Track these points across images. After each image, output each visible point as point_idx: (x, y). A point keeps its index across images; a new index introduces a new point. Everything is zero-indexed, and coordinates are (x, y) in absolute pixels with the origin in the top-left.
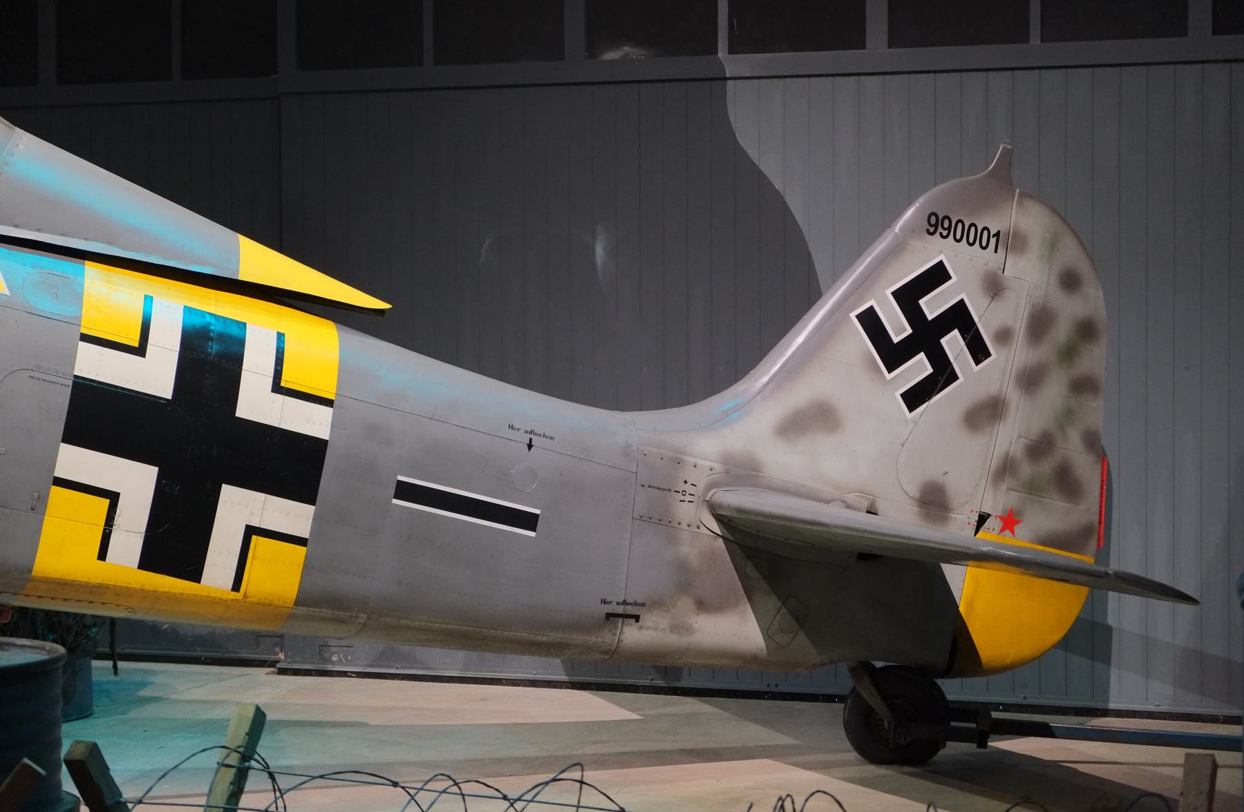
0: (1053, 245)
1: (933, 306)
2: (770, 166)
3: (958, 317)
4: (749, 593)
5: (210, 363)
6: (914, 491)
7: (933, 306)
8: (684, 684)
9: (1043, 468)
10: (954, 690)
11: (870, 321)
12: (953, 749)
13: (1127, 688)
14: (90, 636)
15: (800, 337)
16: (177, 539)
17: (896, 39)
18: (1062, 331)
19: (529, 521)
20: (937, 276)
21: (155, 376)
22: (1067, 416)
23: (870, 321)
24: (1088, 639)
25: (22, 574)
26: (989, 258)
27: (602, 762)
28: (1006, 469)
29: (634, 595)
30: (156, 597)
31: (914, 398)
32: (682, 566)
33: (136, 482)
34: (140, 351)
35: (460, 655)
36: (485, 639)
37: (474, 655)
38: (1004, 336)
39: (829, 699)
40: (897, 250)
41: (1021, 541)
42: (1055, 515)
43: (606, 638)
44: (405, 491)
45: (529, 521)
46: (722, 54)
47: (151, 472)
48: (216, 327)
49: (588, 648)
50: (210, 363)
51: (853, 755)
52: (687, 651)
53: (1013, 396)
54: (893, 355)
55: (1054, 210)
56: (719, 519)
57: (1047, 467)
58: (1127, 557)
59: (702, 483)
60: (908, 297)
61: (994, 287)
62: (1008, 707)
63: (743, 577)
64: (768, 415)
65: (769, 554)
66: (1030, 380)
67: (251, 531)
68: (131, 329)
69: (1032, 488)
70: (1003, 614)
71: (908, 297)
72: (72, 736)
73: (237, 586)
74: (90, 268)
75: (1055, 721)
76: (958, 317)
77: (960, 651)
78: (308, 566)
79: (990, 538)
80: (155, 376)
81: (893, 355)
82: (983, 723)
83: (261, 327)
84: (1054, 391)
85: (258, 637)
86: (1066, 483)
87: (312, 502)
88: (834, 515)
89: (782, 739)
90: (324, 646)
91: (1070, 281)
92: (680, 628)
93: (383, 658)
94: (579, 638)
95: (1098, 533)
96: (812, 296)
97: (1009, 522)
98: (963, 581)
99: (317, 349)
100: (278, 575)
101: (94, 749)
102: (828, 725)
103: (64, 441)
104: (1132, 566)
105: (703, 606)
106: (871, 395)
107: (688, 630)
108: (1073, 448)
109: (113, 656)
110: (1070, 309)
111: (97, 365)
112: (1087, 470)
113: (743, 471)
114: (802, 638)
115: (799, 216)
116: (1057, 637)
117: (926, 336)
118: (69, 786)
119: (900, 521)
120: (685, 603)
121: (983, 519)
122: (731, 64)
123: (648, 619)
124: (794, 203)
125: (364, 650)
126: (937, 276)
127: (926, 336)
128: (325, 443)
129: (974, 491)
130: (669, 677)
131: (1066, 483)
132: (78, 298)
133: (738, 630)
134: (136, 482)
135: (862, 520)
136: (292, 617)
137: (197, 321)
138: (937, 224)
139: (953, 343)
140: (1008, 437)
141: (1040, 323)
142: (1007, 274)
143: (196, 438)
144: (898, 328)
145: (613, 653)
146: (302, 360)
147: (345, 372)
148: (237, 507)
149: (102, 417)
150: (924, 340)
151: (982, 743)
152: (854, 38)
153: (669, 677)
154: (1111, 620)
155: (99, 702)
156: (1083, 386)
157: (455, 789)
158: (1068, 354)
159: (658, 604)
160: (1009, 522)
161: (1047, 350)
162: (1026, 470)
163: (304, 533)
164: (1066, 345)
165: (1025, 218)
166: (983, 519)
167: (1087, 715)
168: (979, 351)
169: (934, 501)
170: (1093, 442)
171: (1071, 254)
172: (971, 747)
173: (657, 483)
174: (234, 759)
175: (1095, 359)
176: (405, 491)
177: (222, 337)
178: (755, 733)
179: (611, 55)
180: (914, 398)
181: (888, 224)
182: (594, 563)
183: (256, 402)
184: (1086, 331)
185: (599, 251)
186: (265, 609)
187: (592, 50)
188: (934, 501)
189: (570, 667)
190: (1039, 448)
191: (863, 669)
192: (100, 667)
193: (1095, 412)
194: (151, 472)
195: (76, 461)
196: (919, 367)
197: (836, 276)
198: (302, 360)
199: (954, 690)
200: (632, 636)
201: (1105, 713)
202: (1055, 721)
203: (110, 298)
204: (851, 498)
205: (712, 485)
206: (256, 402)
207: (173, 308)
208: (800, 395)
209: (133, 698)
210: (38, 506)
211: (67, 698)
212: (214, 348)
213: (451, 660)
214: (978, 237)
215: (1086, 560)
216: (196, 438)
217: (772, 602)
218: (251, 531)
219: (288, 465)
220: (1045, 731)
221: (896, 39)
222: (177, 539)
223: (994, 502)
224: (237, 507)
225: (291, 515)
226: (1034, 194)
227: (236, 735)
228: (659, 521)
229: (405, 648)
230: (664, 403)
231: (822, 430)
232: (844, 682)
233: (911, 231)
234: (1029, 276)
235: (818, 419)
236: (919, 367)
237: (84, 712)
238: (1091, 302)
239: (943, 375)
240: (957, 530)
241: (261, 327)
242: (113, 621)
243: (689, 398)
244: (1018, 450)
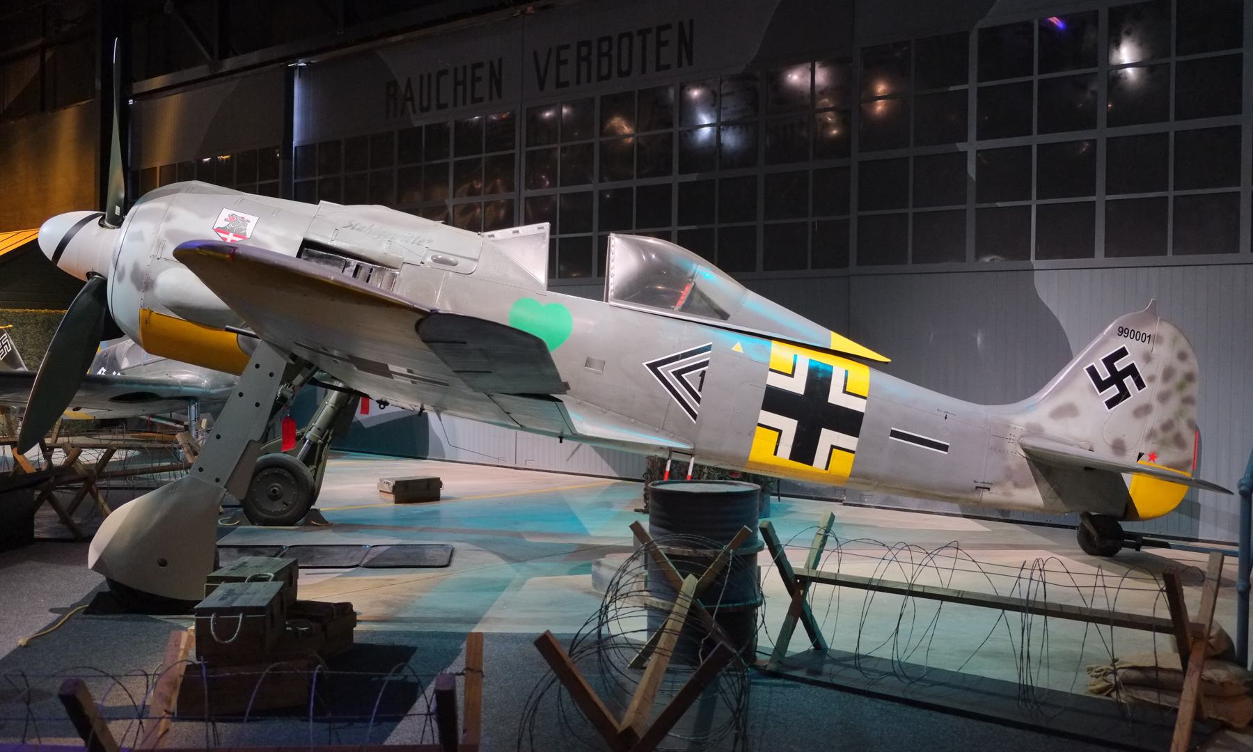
0: (1174, 341)
1: (1120, 365)
2: (1052, 306)
3: (1131, 370)
4: (1037, 481)
5: (819, 381)
6: (1110, 442)
7: (1120, 365)
8: (1011, 518)
9: (1169, 434)
10: (1127, 526)
11: (1092, 371)
12: (1124, 551)
13: (1206, 530)
14: (771, 485)
15: (1061, 377)
16: (804, 449)
17: (1108, 254)
18: (1178, 377)
19: (945, 448)
20: (1122, 353)
21: (797, 385)
22: (1180, 413)
23: (1092, 371)
24: (1189, 508)
25: (745, 460)
26: (1145, 346)
27: (973, 547)
28: (1151, 435)
29: (981, 478)
30: (796, 471)
31: (1111, 403)
32: (1008, 469)
33: (789, 426)
34: (792, 376)
35: (918, 501)
36: (928, 495)
37: (923, 501)
38: (1152, 379)
39: (1073, 528)
40: (1104, 342)
41: (1157, 465)
42: (1172, 455)
43: (976, 496)
44: (894, 434)
45: (945, 448)
46: (1032, 259)
47: (795, 422)
48: (821, 367)
49: (967, 500)
50: (819, 381)
51: (1081, 551)
52: (1009, 504)
53: (1155, 403)
54: (1102, 385)
55: (1175, 326)
56: (1025, 450)
57: (1170, 435)
58: (1207, 475)
59: (1018, 435)
60: (1109, 361)
61: (1148, 358)
62: (1153, 536)
63: (1034, 475)
64: (1047, 408)
65: (1046, 466)
66: (1164, 397)
67: (833, 447)
68: (789, 368)
69: (1163, 443)
70: (1149, 496)
71: (1109, 361)
72: (761, 522)
73: (827, 468)
74: (774, 342)
75: (1171, 542)
76: (1131, 370)
77: (1129, 511)
78: (855, 462)
79: (1144, 463)
80: (797, 385)
81: (1102, 385)
82: (1138, 541)
83: (839, 368)
84: (1174, 402)
85: (835, 489)
86: (1179, 441)
87: (856, 435)
88: (1074, 451)
89: (1051, 543)
90: (862, 495)
91: (1182, 356)
92: (1006, 494)
93: (887, 500)
94: (965, 496)
95: (1196, 461)
96: (1068, 358)
97: (1153, 457)
98: (1130, 480)
99: (861, 377)
100: (843, 465)
101: (770, 524)
102: (1071, 537)
103: (763, 408)
104: (1210, 479)
105: (1016, 485)
106: (1093, 402)
107: (1010, 494)
108: (1182, 427)
109: (779, 495)
110: (1182, 368)
111: (776, 381)
112: (1189, 436)
113: (1035, 431)
114: (1060, 500)
115: (1064, 327)
116: (1173, 506)
117: (1117, 378)
118: (760, 536)
119: (1103, 454)
120: (1009, 484)
121: (1140, 455)
122: (1036, 263)
123: (993, 490)
124: (1062, 322)
125: (878, 496)
126: (1122, 353)
127: (1117, 378)
128: (862, 414)
129: (1137, 442)
130: (1005, 515)
131: (1179, 441)
132: (769, 354)
133: (1032, 496)
134: (789, 426)
135: (1086, 453)
136: (848, 481)
137: (814, 365)
138: (1122, 331)
139: (1129, 381)
140: (1153, 421)
141: (1168, 374)
142: (1155, 353)
143: (813, 411)
144: (1105, 374)
145: (978, 503)
146: (854, 382)
147: (872, 386)
148: (828, 437)
149: (776, 401)
150: (1116, 379)
151: (1138, 549)
152: (1090, 253)
153: (1005, 515)
154: (1200, 501)
155: (772, 512)
156: (1188, 401)
157: (931, 563)
158: (1181, 387)
159: (998, 484)
160: (1153, 457)
161: (1170, 385)
162: (1161, 435)
163: (854, 449)
164: (1180, 384)
165: (1163, 329)
166: (1140, 455)
167: (1188, 541)
168: (1140, 384)
169: (1119, 447)
170: (1192, 425)
171: (1183, 344)
172: (1132, 551)
173: (997, 438)
174: (822, 532)
175: (1193, 390)
176: (894, 434)
177: (824, 371)
178: (1039, 539)
179: (987, 259)
180: (1111, 403)
181: (1101, 331)
182: (968, 466)
183: (836, 397)
184: (1189, 377)
185: (979, 340)
186: (837, 478)
187: (977, 257)
188: (1119, 447)
189: (963, 508)
190: (1167, 426)
191: (1086, 515)
192: (773, 498)
193: (1192, 412)
194: (795, 422)
195: (767, 417)
196: (1114, 391)
197: (1079, 352)
198: (854, 382)
199: (1127, 526)
200: (987, 496)
201: (1197, 540)
202: (1171, 542)
203: (781, 355)
204: (1082, 444)
205: (1022, 436)
206: (836, 397)
207: (805, 359)
208: (1061, 400)
209: (786, 511)
210: (752, 434)
211: (761, 510)
212: (820, 375)
213: (913, 503)
214: (1141, 337)
215: (1188, 475)
216: (813, 411)
217: (1047, 485)
218: (833, 447)
219: (849, 422)
220: (1167, 546)
221: (1108, 254)
222: (804, 449)
223: (1146, 448)
224: (828, 437)
225: (849, 441)
226: (1169, 320)
227: (824, 523)
228: (999, 450)
229: (894, 497)
230: (1005, 402)
231: (1070, 415)
232: (1078, 521)
233: (1111, 334)
234: (1164, 354)
235: (1068, 411)
236: (1114, 391)
237: (767, 516)
238: (1192, 365)
239: (1124, 394)
240: (1129, 459)
241: (839, 368)
242: (779, 480)
243: (1015, 400)
244: (1157, 426)
